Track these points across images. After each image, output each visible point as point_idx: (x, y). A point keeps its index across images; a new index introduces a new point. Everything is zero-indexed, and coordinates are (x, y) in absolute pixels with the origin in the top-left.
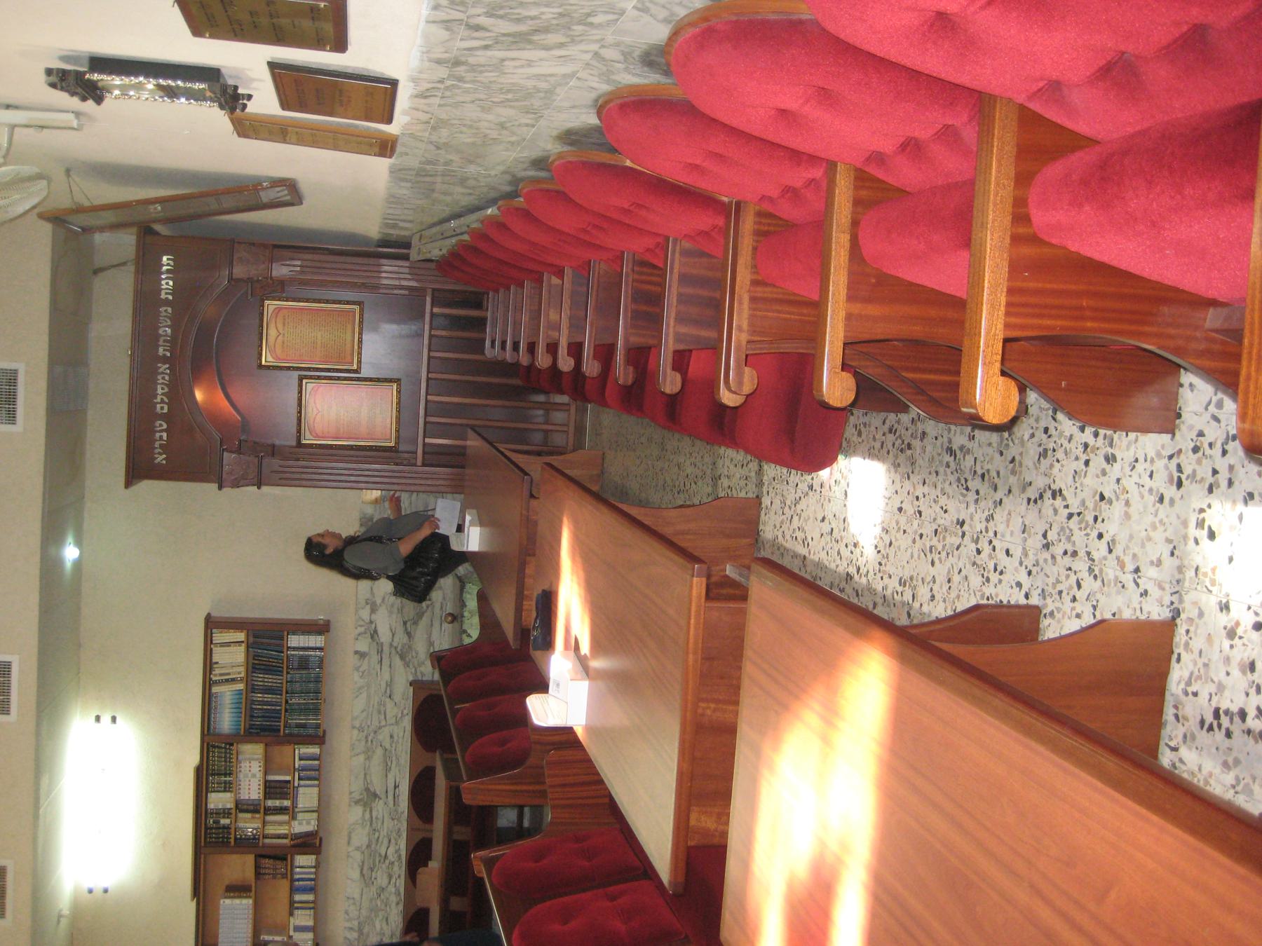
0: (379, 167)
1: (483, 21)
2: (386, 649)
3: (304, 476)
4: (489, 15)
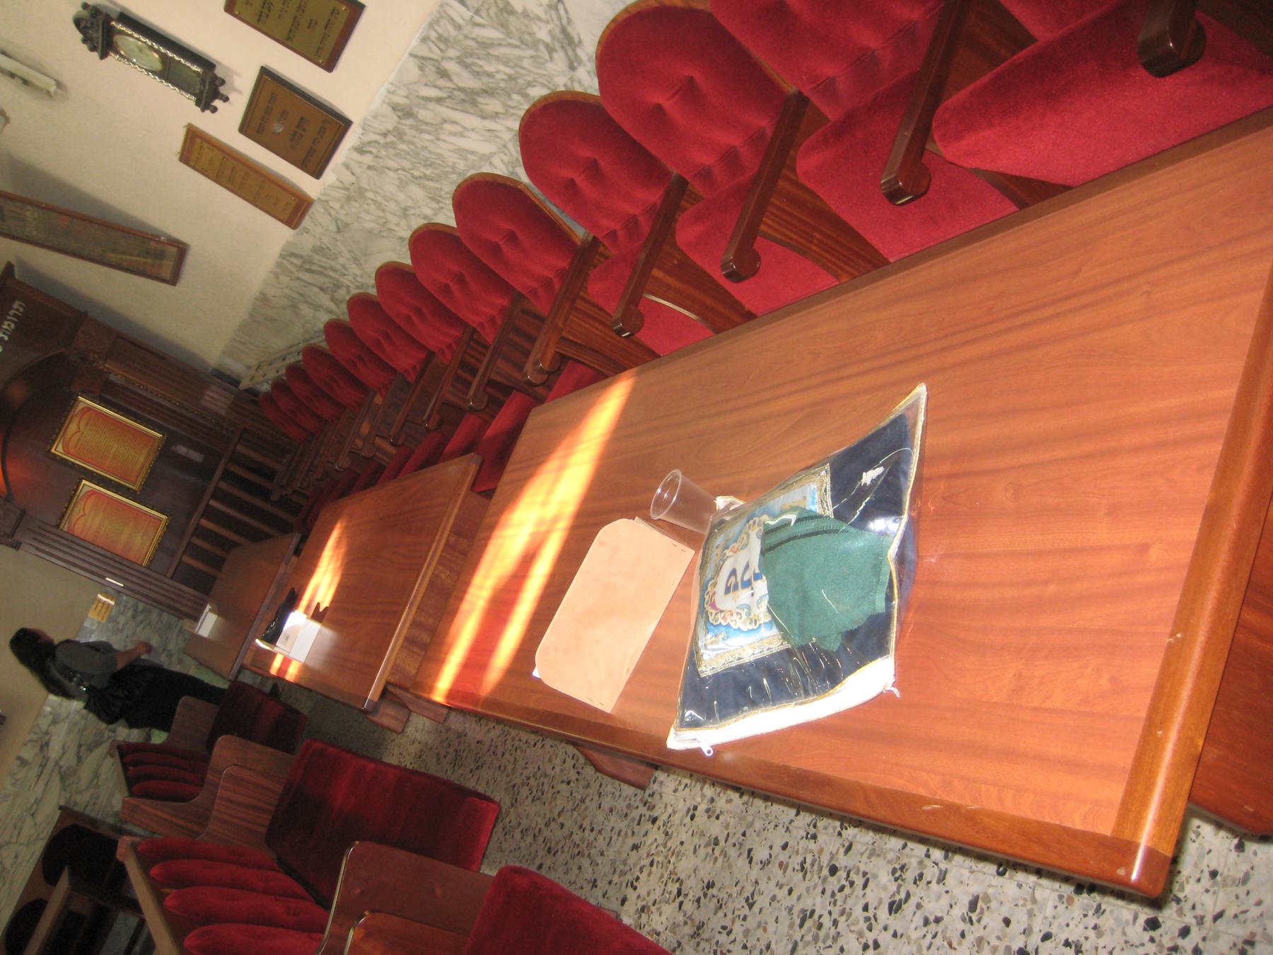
0: (276, 234)
1: (451, 67)
2: (50, 765)
3: (56, 545)
4: (460, 61)
